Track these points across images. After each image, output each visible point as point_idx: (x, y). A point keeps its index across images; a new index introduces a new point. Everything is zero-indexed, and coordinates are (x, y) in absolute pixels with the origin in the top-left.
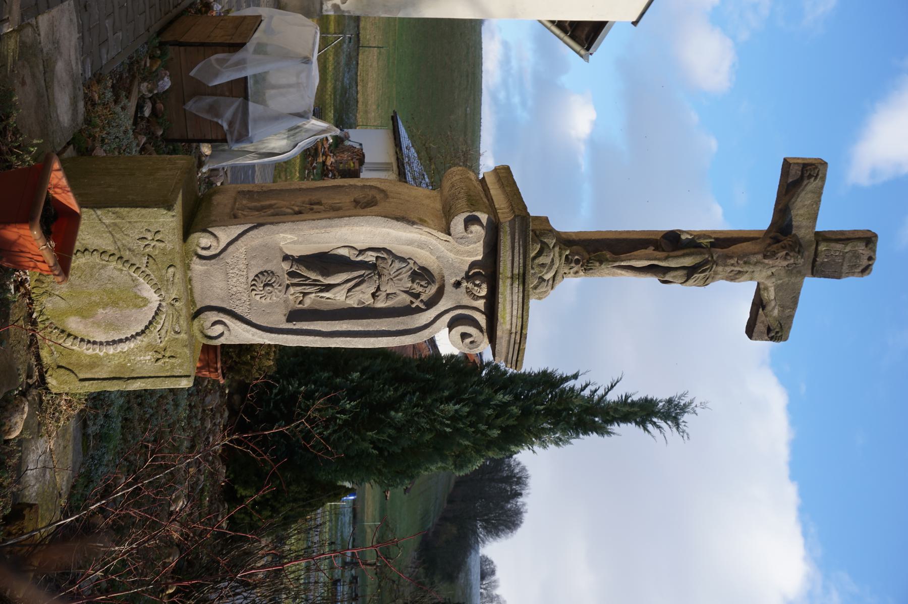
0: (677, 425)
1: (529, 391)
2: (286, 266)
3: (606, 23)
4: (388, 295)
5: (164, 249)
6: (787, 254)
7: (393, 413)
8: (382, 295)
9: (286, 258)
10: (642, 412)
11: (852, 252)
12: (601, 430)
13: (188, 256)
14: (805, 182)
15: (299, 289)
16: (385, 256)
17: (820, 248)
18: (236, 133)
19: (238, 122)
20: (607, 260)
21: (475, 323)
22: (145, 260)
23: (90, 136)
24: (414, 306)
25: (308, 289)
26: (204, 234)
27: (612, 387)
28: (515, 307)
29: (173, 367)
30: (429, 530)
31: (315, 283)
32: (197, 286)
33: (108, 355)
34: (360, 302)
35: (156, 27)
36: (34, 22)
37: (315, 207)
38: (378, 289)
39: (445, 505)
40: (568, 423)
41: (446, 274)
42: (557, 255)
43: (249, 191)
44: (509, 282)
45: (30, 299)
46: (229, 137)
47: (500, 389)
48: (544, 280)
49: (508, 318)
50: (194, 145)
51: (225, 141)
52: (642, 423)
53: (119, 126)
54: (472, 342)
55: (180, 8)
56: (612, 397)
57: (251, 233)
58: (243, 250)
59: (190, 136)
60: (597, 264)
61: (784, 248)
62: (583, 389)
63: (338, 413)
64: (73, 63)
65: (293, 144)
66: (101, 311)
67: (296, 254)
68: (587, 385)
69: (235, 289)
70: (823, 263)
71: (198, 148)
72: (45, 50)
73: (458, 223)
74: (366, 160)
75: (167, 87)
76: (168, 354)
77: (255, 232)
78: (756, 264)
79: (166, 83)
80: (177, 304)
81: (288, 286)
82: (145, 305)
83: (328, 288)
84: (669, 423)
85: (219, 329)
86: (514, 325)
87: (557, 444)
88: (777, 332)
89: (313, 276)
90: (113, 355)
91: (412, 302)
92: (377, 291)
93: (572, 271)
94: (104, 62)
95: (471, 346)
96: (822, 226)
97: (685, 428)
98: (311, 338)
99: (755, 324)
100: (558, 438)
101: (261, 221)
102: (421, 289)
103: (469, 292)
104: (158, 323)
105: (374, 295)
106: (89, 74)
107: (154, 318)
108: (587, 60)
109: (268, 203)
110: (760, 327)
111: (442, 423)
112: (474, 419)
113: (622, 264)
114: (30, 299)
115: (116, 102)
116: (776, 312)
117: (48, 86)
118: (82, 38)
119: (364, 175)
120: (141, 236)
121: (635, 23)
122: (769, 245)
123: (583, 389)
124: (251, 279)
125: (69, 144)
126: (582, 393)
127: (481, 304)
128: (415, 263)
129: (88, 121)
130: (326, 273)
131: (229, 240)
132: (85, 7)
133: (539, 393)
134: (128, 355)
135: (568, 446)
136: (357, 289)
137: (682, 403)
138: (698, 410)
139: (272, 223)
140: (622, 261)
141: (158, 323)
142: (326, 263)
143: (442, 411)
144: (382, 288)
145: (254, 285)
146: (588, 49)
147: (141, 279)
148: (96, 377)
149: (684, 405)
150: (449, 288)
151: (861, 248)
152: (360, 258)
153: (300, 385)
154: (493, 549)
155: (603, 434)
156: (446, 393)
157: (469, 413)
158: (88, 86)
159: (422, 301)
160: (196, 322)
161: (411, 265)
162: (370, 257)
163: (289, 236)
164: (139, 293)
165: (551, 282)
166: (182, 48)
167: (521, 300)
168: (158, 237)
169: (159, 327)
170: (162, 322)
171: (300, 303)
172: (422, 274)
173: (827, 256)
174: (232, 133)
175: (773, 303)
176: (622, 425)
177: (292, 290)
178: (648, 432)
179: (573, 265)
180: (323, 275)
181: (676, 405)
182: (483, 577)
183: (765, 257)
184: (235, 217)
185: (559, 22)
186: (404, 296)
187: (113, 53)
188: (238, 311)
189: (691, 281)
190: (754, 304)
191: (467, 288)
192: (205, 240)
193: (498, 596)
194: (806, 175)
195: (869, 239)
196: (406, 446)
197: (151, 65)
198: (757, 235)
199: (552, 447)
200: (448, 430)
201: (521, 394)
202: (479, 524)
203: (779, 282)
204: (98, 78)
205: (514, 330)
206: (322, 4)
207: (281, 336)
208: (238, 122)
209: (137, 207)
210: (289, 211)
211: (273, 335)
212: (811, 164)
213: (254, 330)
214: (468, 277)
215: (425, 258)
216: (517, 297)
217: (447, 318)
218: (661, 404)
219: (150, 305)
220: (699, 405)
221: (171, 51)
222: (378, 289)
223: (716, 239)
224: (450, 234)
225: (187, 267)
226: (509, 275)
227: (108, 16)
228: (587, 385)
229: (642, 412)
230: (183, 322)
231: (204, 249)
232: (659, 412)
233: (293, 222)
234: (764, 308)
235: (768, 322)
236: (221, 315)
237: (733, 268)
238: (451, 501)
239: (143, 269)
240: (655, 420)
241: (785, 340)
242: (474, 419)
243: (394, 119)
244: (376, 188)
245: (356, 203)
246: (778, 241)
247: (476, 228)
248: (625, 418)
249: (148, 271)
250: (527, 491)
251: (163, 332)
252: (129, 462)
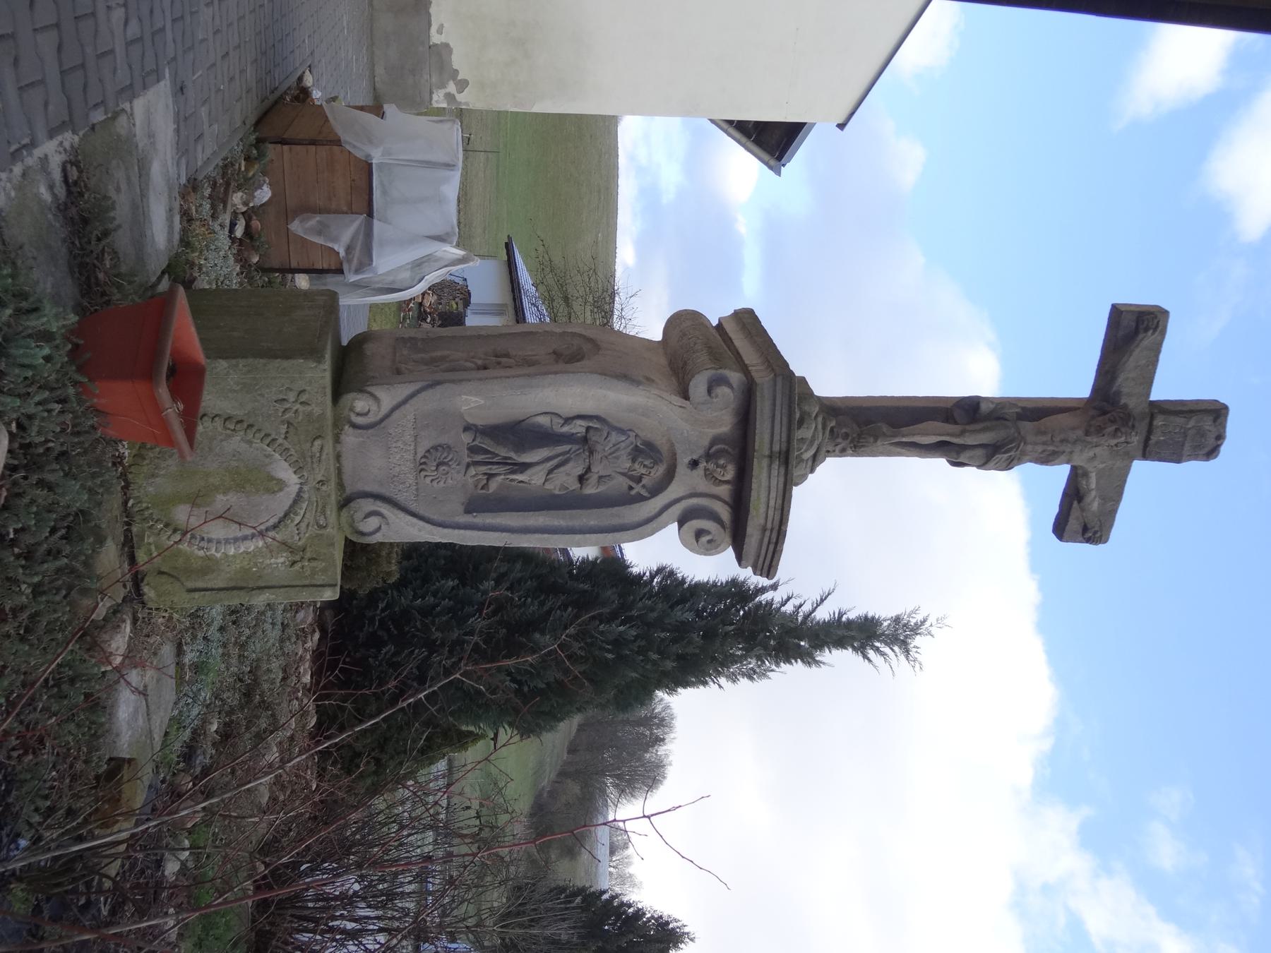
0: (907, 652)
1: (714, 606)
2: (467, 438)
3: (804, 124)
4: (600, 477)
5: (309, 415)
6: (1117, 430)
7: (537, 636)
8: (593, 478)
9: (467, 428)
10: (861, 634)
11: (1195, 430)
12: (808, 658)
13: (339, 424)
14: (1141, 336)
15: (483, 469)
16: (597, 426)
17: (1155, 423)
18: (355, 261)
19: (358, 248)
20: (884, 435)
21: (714, 517)
22: (283, 428)
23: (187, 261)
24: (633, 492)
25: (495, 469)
26: (360, 396)
27: (822, 600)
28: (773, 494)
29: (314, 572)
30: (543, 788)
31: (504, 462)
32: (347, 465)
33: (226, 555)
34: (563, 487)
35: (252, 119)
36: (127, 106)
37: (504, 360)
38: (588, 470)
39: (565, 756)
40: (766, 648)
41: (679, 449)
42: (820, 427)
43: (411, 338)
44: (765, 462)
45: (126, 481)
46: (345, 267)
47: (678, 603)
48: (802, 460)
49: (762, 510)
50: (290, 276)
51: (340, 271)
52: (861, 650)
53: (217, 249)
54: (709, 542)
55: (277, 94)
56: (823, 614)
57: (423, 394)
58: (411, 417)
59: (294, 265)
60: (872, 440)
61: (1113, 422)
62: (784, 603)
63: (466, 634)
64: (169, 163)
65: (418, 278)
66: (220, 497)
67: (479, 422)
68: (789, 599)
69: (397, 469)
70: (1157, 442)
71: (293, 280)
72: (140, 145)
73: (698, 386)
74: (473, 300)
75: (265, 199)
76: (308, 555)
77: (430, 391)
78: (1075, 442)
79: (264, 194)
80: (324, 488)
81: (468, 466)
82: (281, 490)
83: (524, 467)
84: (896, 648)
85: (373, 523)
86: (770, 518)
87: (751, 678)
88: (1095, 533)
89: (503, 452)
90: (234, 556)
91: (631, 488)
92: (586, 472)
93: (838, 448)
94: (200, 163)
95: (709, 546)
96: (1159, 392)
97: (917, 655)
98: (497, 534)
99: (1066, 521)
100: (752, 669)
101: (438, 377)
102: (643, 471)
103: (708, 475)
104: (296, 514)
105: (582, 479)
106: (183, 180)
107: (291, 506)
108: (778, 173)
109: (439, 353)
110: (1073, 524)
111: (601, 648)
112: (643, 643)
113: (904, 440)
114: (126, 481)
115: (214, 217)
116: (1095, 506)
117: (144, 195)
118: (177, 131)
119: (472, 320)
120: (281, 397)
121: (841, 126)
122: (1093, 417)
123: (784, 603)
124: (419, 456)
125: (163, 273)
126: (783, 609)
127: (724, 491)
128: (637, 436)
129: (185, 242)
130: (521, 447)
131: (395, 403)
132: (182, 89)
133: (727, 608)
134: (255, 556)
135: (765, 681)
136: (562, 469)
137: (913, 622)
138: (933, 630)
139: (453, 381)
140: (903, 436)
141: (296, 514)
142: (520, 434)
143: (602, 633)
144: (594, 469)
145: (424, 463)
146: (779, 158)
147: (277, 456)
148: (209, 586)
149: (916, 624)
150: (682, 469)
151: (1207, 423)
152: (566, 429)
153: (415, 597)
154: (625, 811)
155: (809, 664)
156: (606, 610)
157: (637, 637)
158: (183, 196)
159: (644, 486)
160: (344, 513)
161: (632, 439)
162: (578, 428)
163: (474, 399)
164: (273, 474)
165: (810, 463)
166: (286, 147)
167: (781, 486)
168: (304, 398)
169: (298, 519)
170: (302, 512)
171: (482, 488)
172: (645, 451)
173: (1164, 434)
174: (349, 261)
175: (1093, 493)
176: (834, 651)
177: (472, 471)
178: (870, 660)
179: (839, 440)
180: (516, 452)
181: (905, 625)
182: (612, 853)
183: (1087, 433)
184: (399, 372)
185: (739, 122)
186: (621, 479)
187: (209, 152)
188: (401, 498)
189: (992, 464)
190: (1066, 494)
191: (706, 470)
192: (361, 404)
193: (631, 876)
194: (1141, 327)
195: (1216, 413)
196: (552, 680)
197: (247, 170)
198: (1075, 405)
199: (744, 681)
200: (610, 656)
201: (704, 609)
202: (609, 781)
203: (1101, 466)
204: (193, 185)
205: (769, 526)
206: (431, 93)
207: (456, 531)
208: (358, 248)
209: (276, 358)
210: (469, 364)
211: (446, 531)
212: (1152, 313)
213: (421, 523)
214: (708, 456)
215: (652, 430)
216: (777, 481)
217: (677, 510)
218: (885, 624)
219: (287, 489)
220: (934, 623)
221: (272, 151)
222: (588, 470)
223: (1024, 409)
224: (686, 397)
225: (337, 440)
226: (767, 453)
227: (203, 104)
228: (789, 599)
229: (861, 634)
230: (331, 513)
231: (358, 414)
232: (883, 634)
233: (480, 379)
234: (1079, 502)
235: (1082, 518)
236: (379, 503)
237: (1045, 447)
238: (572, 750)
239: (280, 441)
240: (877, 644)
241: (1105, 542)
242: (643, 643)
243: (509, 247)
244: (580, 336)
245: (557, 355)
246: (1104, 413)
247: (723, 391)
248: (841, 643)
249: (286, 445)
250: (672, 736)
251: (303, 525)
252: (222, 700)
